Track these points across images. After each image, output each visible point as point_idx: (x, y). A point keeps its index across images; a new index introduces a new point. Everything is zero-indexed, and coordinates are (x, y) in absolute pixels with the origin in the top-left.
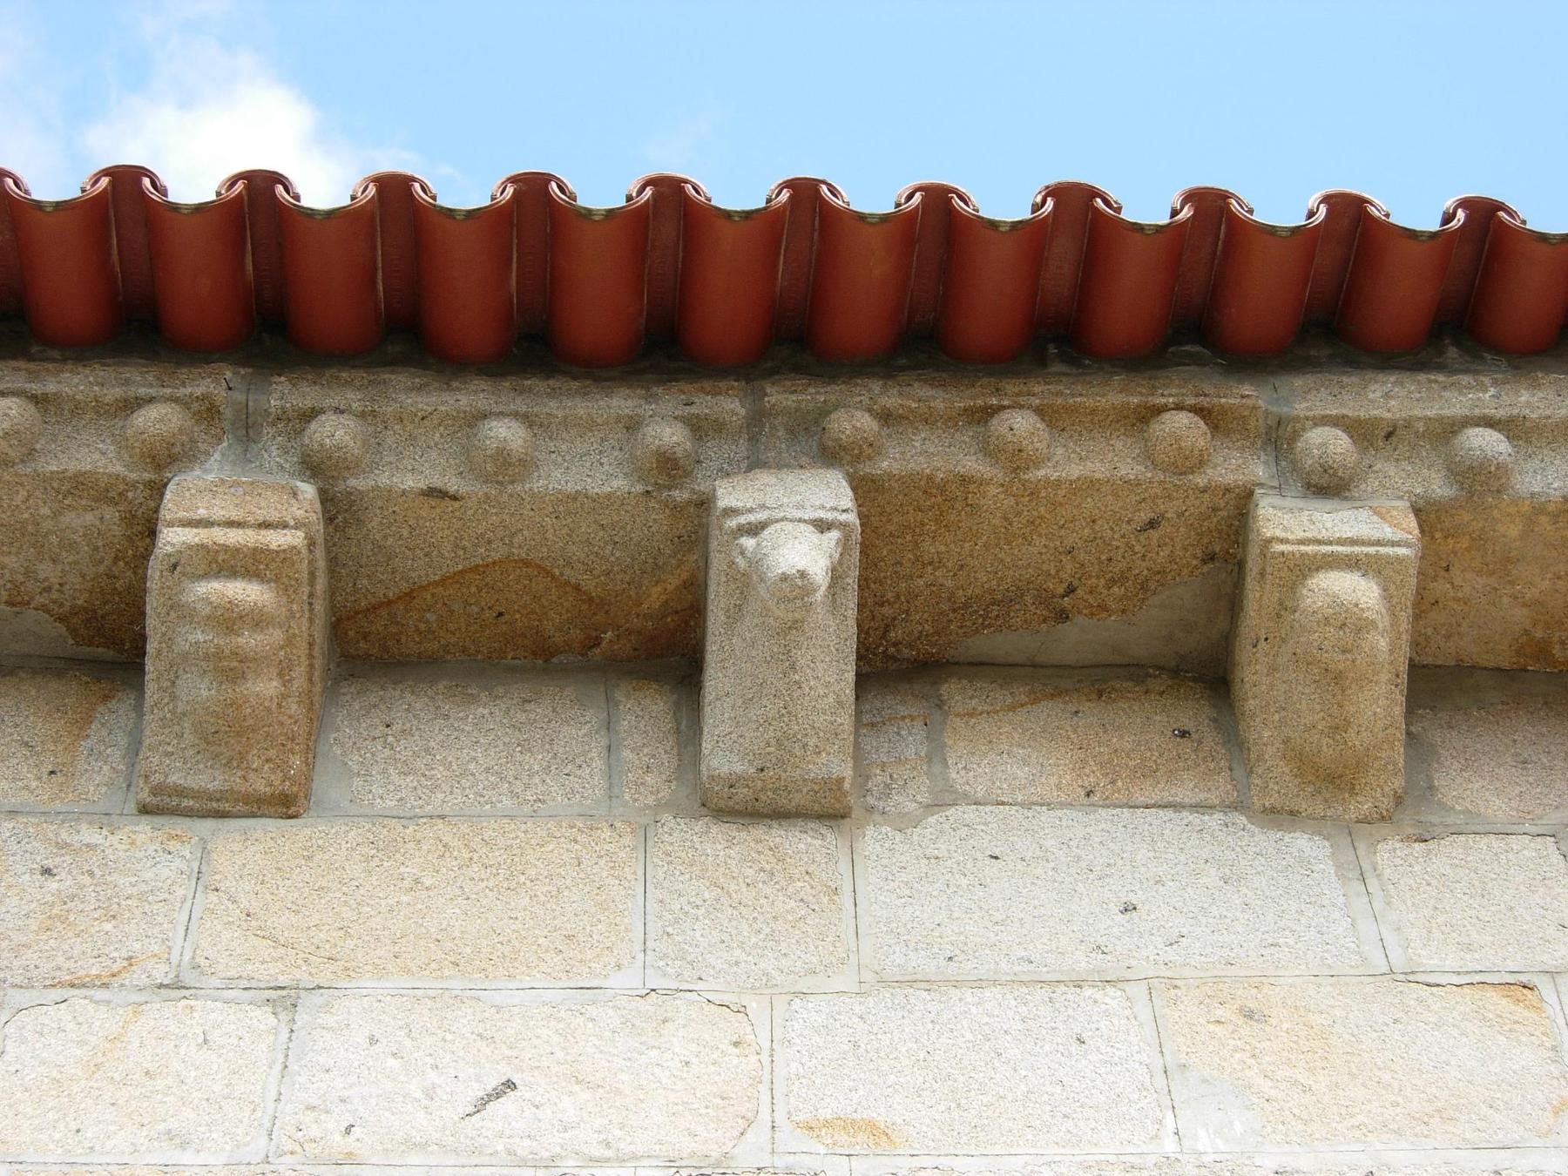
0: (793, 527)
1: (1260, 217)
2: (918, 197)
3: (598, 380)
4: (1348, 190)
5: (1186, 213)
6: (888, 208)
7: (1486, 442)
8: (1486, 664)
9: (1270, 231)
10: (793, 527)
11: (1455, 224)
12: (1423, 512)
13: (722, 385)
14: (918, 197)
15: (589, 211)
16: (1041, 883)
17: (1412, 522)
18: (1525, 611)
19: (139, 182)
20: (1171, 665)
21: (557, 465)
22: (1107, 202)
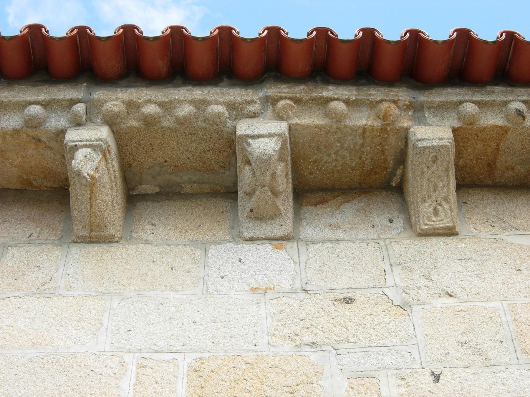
0: (433, 133)
1: (242, 35)
2: (408, 35)
3: (53, 83)
4: (274, 25)
5: (216, 33)
6: (398, 38)
7: (340, 106)
8: (11, 188)
9: (388, 42)
10: (433, 133)
11: (263, 35)
12: (455, 131)
13: (169, 85)
14: (408, 35)
15: (148, 37)
16: (349, 256)
17: (451, 135)
18: (17, 169)
19: (134, 32)
20: (375, 182)
21: (351, 112)
22: (332, 33)
